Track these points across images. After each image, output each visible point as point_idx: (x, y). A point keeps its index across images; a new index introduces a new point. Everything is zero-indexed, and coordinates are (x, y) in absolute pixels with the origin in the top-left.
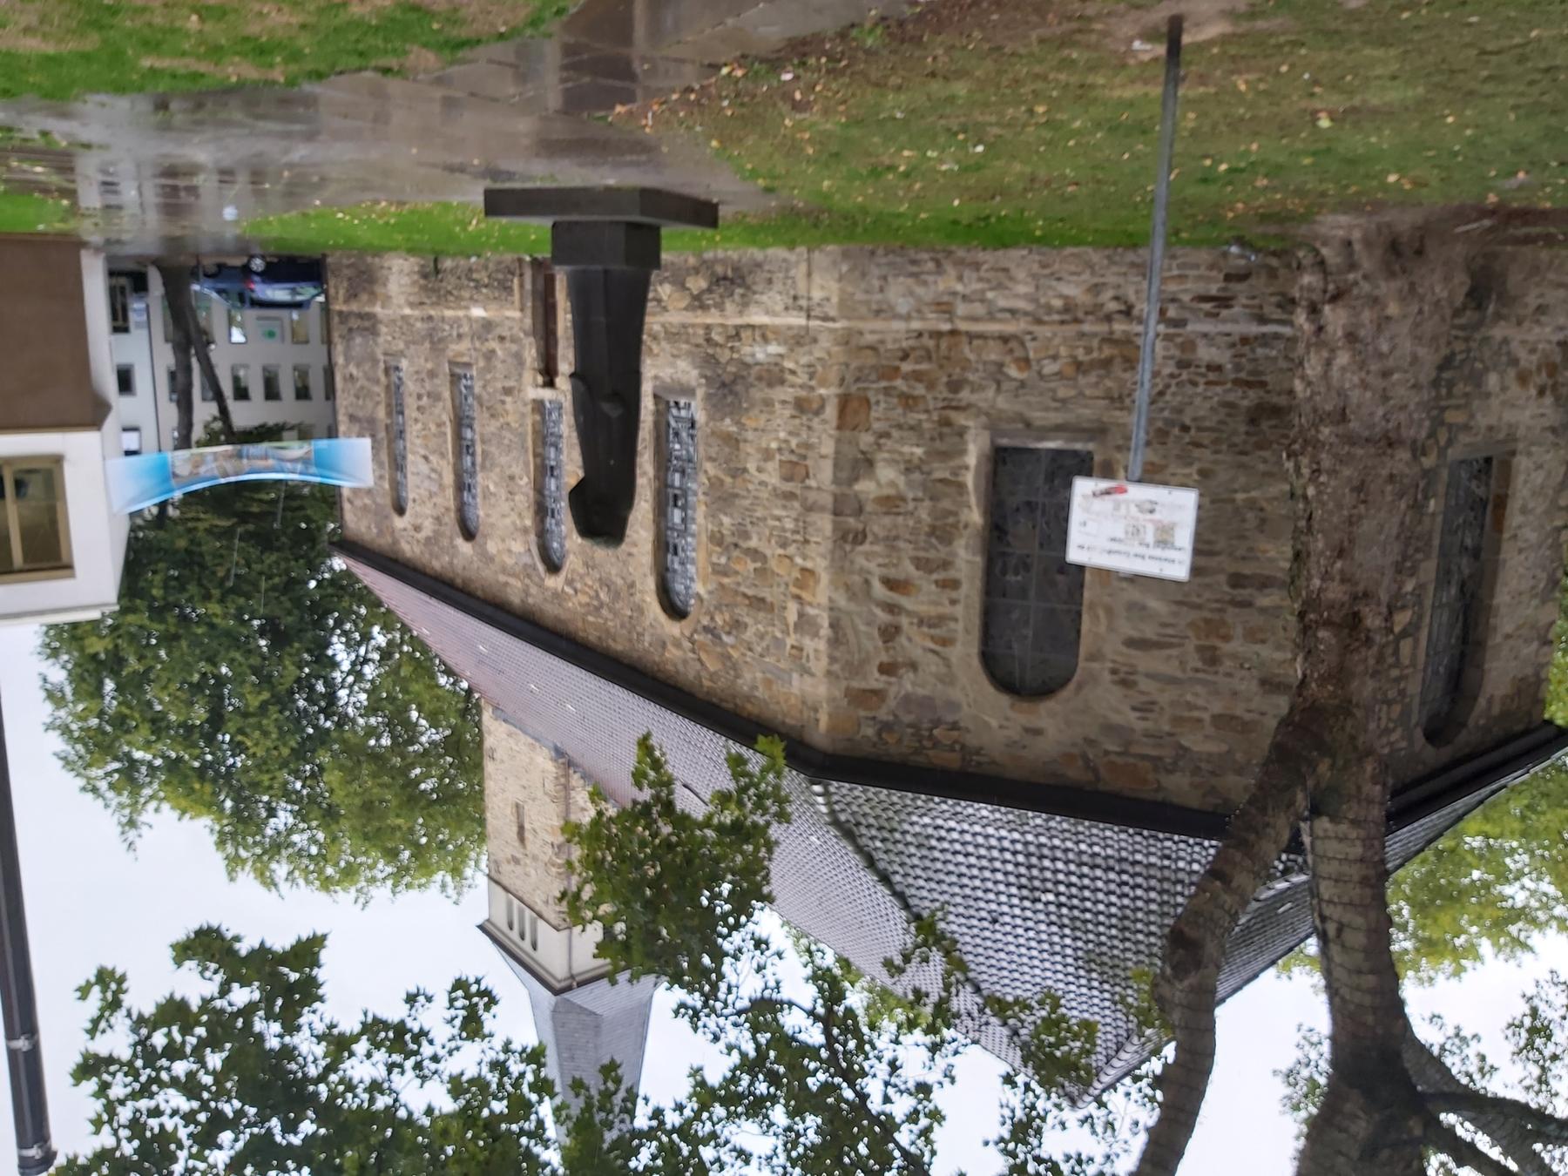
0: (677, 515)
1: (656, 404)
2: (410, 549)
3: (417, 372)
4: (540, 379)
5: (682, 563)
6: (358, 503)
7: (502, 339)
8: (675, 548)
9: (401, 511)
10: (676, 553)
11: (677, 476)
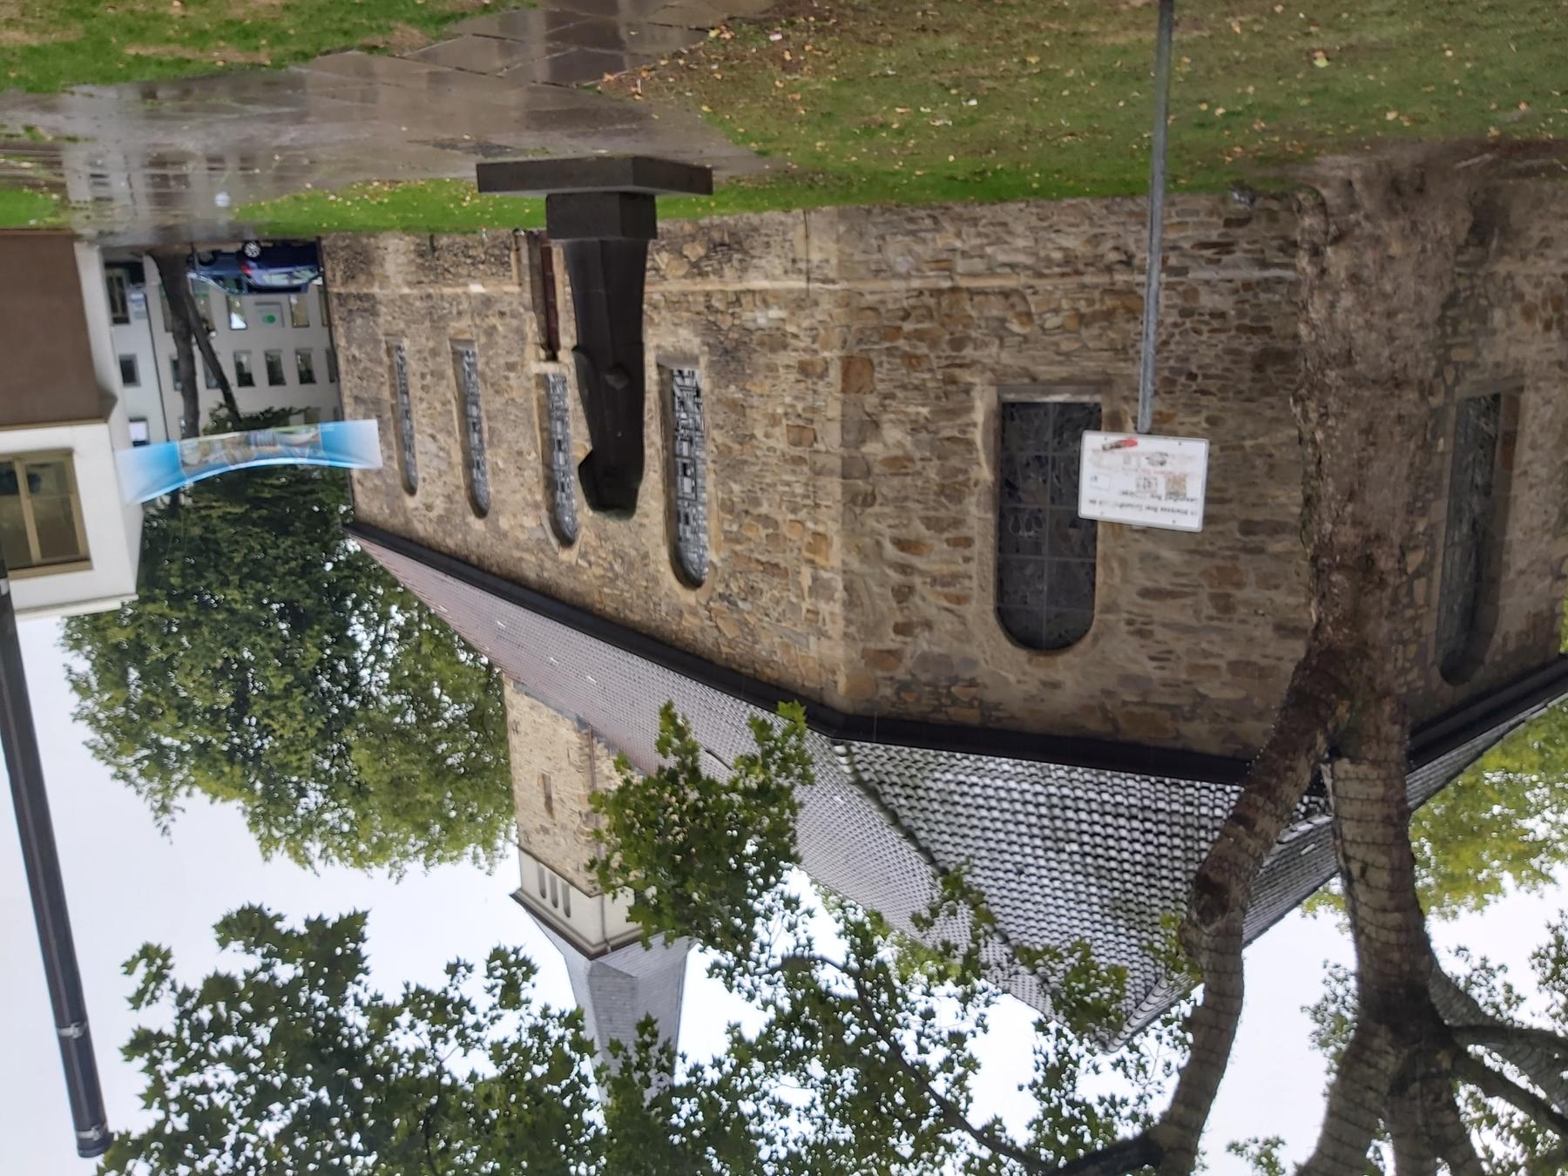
0: (687, 484)
1: (660, 374)
2: (423, 528)
3: (419, 352)
4: (542, 354)
5: (694, 532)
6: (369, 484)
7: (502, 314)
8: (687, 517)
9: (411, 491)
10: (687, 523)
11: (685, 445)
